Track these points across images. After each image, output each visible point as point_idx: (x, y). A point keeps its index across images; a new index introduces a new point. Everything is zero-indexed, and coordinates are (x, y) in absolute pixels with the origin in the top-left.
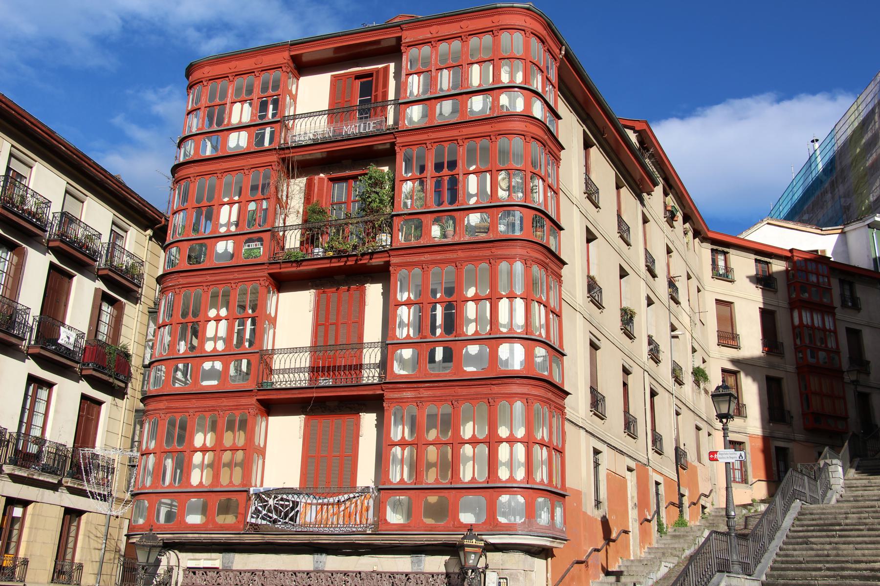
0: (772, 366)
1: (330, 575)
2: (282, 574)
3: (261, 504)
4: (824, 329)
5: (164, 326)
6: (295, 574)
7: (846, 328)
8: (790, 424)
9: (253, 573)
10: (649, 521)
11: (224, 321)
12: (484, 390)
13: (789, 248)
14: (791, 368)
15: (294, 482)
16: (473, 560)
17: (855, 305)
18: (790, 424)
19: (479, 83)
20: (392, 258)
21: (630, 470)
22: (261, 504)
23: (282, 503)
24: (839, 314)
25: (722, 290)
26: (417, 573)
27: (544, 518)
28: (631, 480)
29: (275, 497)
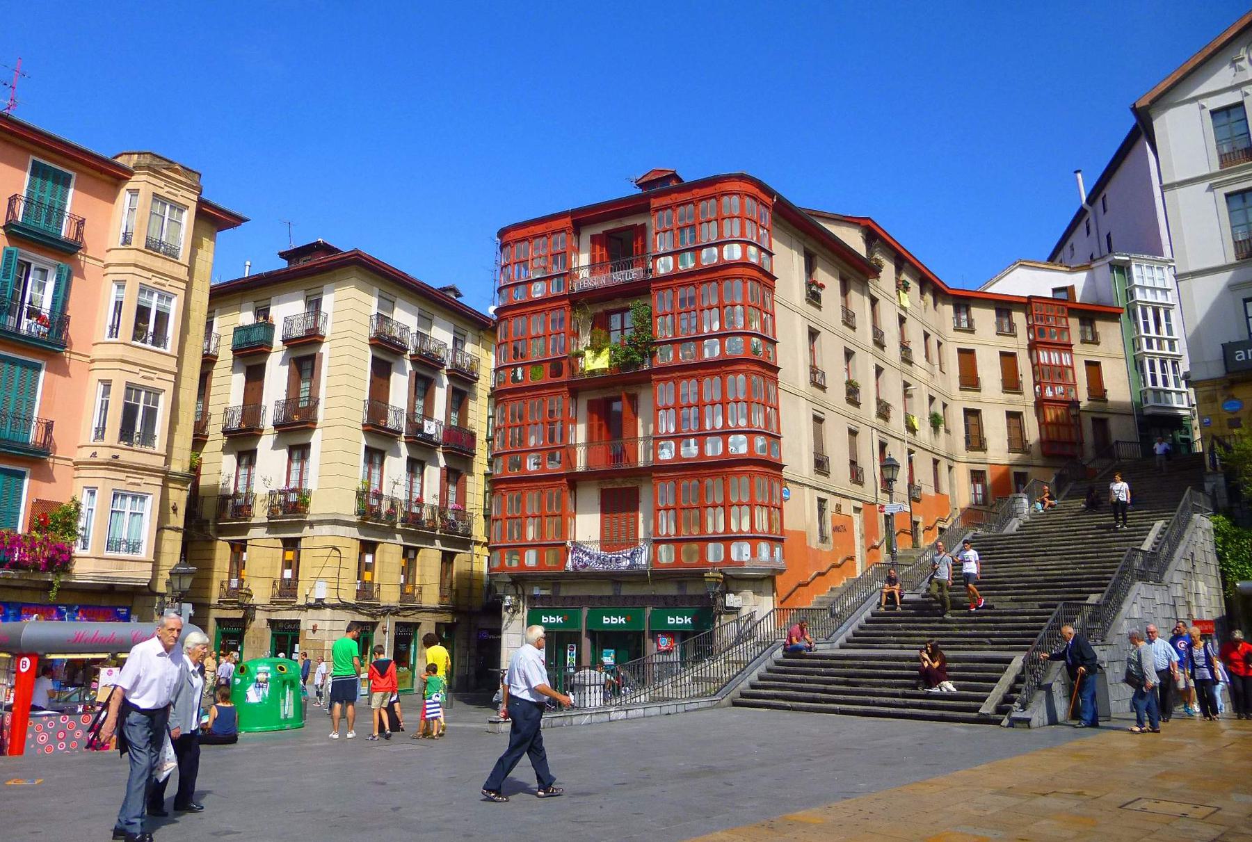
0: (1011, 402)
4: (1062, 366)
5: (497, 520)
7: (1086, 361)
10: (877, 548)
13: (1027, 295)
17: (1095, 341)
21: (857, 510)
24: (1077, 347)
25: (965, 341)
26: (681, 596)
28: (857, 519)
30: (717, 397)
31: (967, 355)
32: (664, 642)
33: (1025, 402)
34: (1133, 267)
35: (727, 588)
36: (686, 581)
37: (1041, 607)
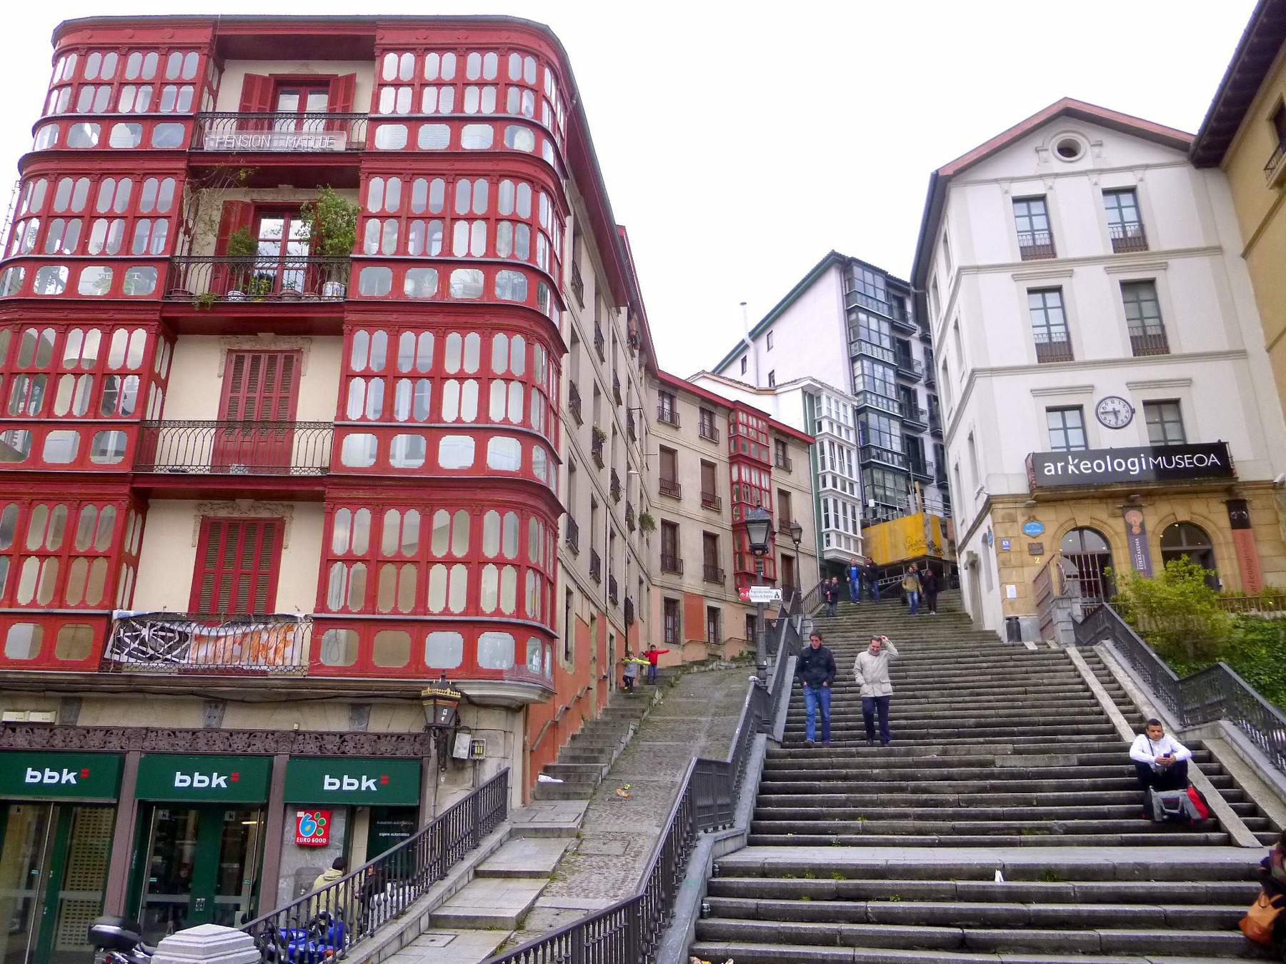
1: (227, 735)
2: (154, 734)
3: (129, 634)
6: (174, 733)
8: (722, 584)
9: (107, 731)
11: (85, 376)
12: (468, 495)
14: (727, 524)
15: (180, 605)
16: (446, 717)
18: (722, 584)
19: (31, 597)
20: (346, 314)
22: (129, 634)
23: (164, 634)
25: (664, 436)
26: (356, 734)
27: (534, 663)
29: (152, 626)
30: (472, 367)
31: (668, 454)
32: (309, 825)
33: (722, 524)
34: (824, 399)
35: (458, 721)
36: (370, 705)
37: (1081, 763)
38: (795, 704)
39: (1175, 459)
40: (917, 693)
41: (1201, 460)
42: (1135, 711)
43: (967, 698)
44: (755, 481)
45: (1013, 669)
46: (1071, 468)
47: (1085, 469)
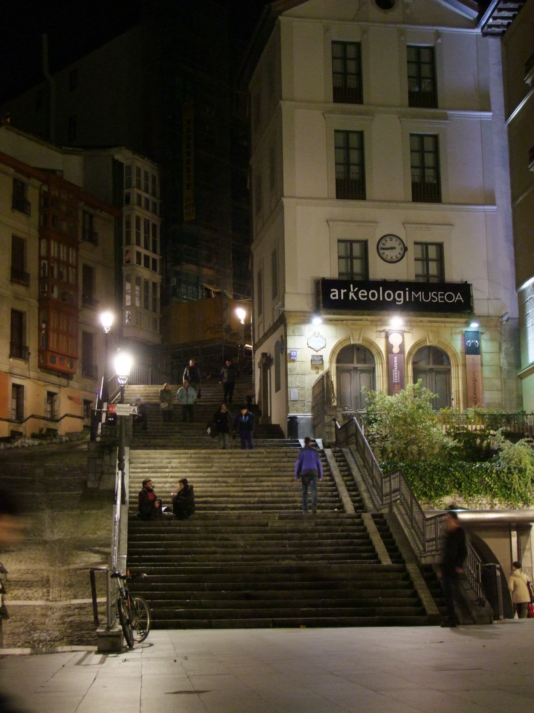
38: (133, 485)
39: (431, 294)
40: (219, 479)
41: (450, 297)
42: (358, 495)
43: (254, 484)
44: (63, 256)
45: (286, 464)
46: (351, 294)
47: (363, 297)
